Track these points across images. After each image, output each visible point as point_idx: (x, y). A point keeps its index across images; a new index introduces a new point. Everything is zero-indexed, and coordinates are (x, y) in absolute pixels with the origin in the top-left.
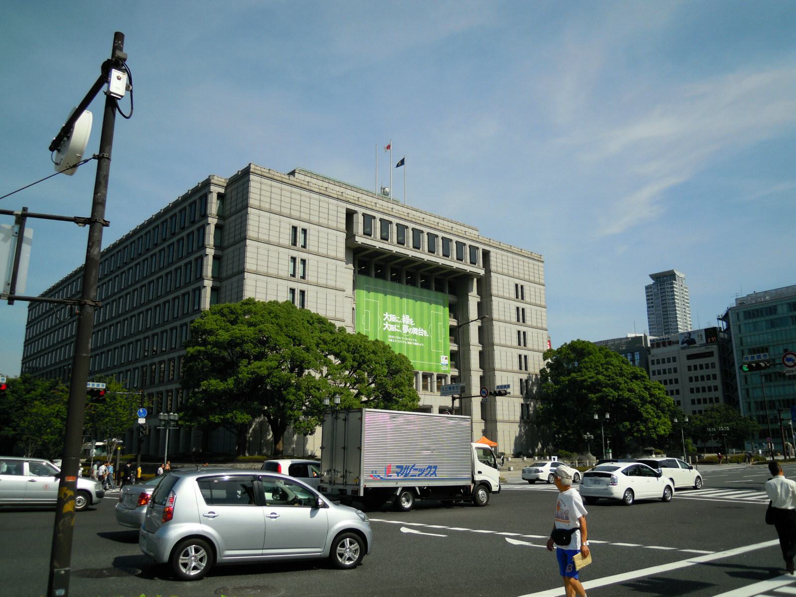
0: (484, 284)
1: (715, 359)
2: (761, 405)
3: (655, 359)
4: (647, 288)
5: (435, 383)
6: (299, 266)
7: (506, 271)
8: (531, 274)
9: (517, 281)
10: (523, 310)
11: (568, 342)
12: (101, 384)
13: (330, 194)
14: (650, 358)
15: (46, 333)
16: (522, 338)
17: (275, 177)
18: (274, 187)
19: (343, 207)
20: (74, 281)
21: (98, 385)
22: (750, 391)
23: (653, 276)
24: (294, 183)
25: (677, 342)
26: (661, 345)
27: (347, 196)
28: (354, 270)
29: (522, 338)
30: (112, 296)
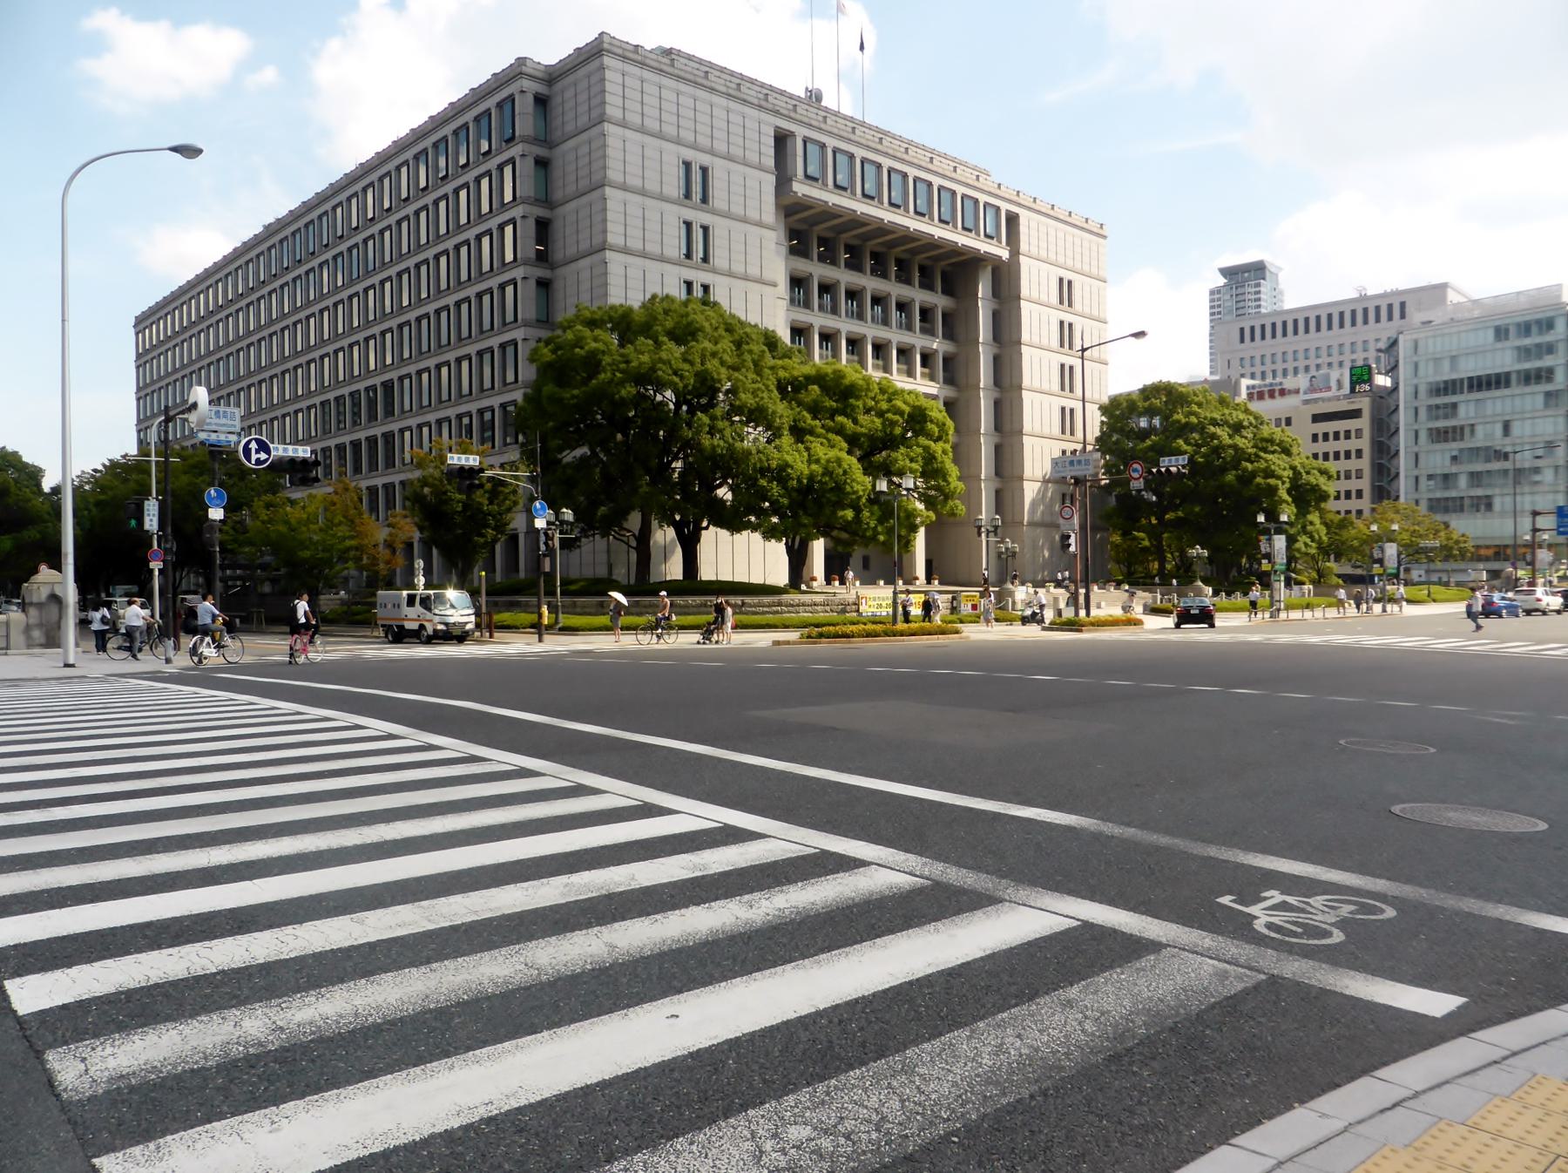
0: (1005, 279)
1: (1364, 423)
4: (1212, 292)
6: (698, 235)
9: (689, 154)
11: (10, 448)
12: (300, 448)
16: (1066, 376)
18: (683, 93)
19: (769, 124)
23: (1228, 272)
25: (1297, 391)
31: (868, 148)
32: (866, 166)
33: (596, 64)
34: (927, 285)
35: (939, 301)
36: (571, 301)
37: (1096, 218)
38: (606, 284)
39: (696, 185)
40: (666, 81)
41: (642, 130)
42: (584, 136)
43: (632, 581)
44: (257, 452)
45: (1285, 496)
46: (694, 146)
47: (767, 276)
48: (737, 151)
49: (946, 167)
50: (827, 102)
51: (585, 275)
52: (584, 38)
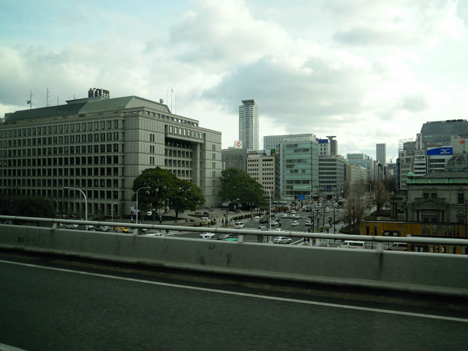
0: (202, 145)
2: (289, 182)
3: (250, 159)
9: (151, 133)
14: (248, 159)
22: (285, 171)
23: (244, 102)
25: (260, 154)
26: (253, 154)
35: (189, 150)
39: (152, 138)
41: (144, 130)
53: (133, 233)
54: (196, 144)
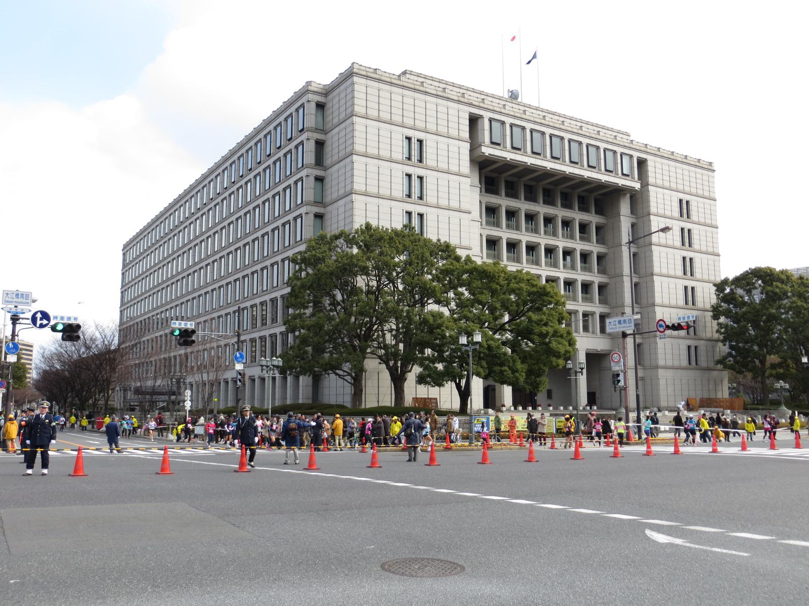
0: (638, 199)
5: (581, 321)
6: (416, 183)
7: (667, 184)
8: (700, 186)
9: (682, 196)
10: (689, 231)
12: (189, 323)
13: (449, 96)
15: (154, 269)
16: (688, 266)
17: (383, 78)
18: (395, 93)
20: (176, 210)
21: (186, 324)
24: (406, 84)
27: (470, 98)
28: (481, 188)
29: (688, 266)
30: (212, 228)
31: (608, 142)
32: (607, 152)
33: (349, 82)
34: (584, 208)
35: (593, 219)
36: (335, 226)
37: (706, 158)
38: (352, 215)
39: (416, 150)
40: (370, 83)
42: (343, 125)
43: (393, 405)
44: (41, 319)
45: (298, 312)
46: (414, 128)
47: (464, 207)
48: (442, 129)
49: (609, 136)
50: (524, 98)
51: (342, 210)
52: (343, 68)
53: (613, 455)
54: (616, 192)
